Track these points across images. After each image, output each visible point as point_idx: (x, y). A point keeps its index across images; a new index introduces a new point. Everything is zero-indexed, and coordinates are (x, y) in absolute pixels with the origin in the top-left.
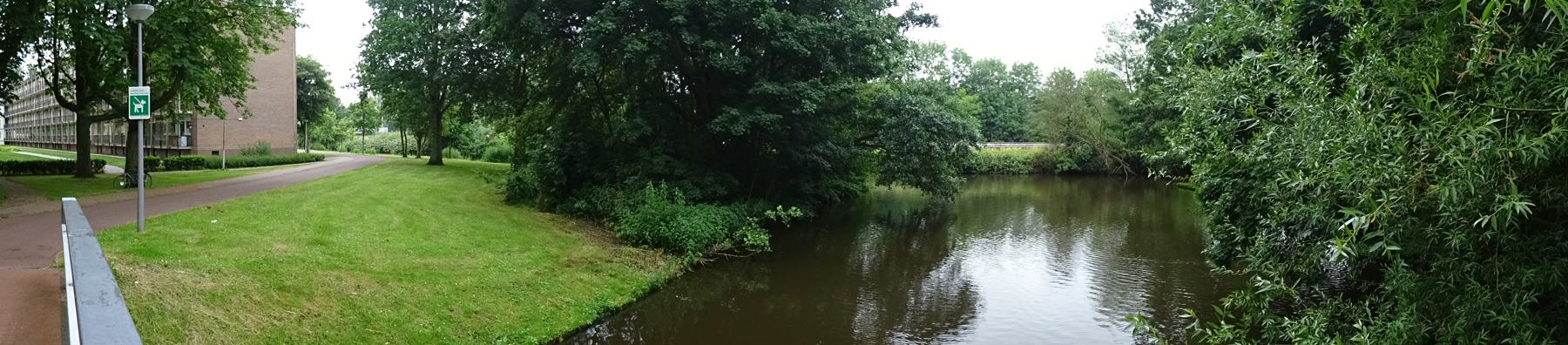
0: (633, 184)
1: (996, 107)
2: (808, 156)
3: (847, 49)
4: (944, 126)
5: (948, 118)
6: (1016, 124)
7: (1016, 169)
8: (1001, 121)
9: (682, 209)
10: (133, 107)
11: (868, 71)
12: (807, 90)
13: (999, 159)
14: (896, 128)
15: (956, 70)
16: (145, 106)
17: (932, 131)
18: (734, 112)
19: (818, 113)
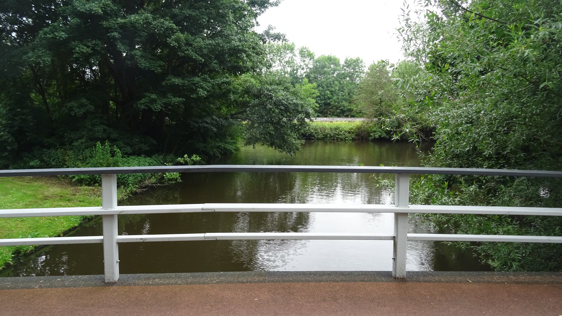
0: (79, 146)
1: (331, 92)
2: (201, 125)
3: (226, 56)
4: (289, 105)
5: (292, 100)
6: (345, 104)
7: (343, 137)
8: (335, 102)
9: (120, 159)
11: (237, 70)
12: (200, 82)
13: (331, 129)
14: (258, 106)
15: (302, 64)
17: (280, 109)
18: (153, 96)
19: (206, 98)
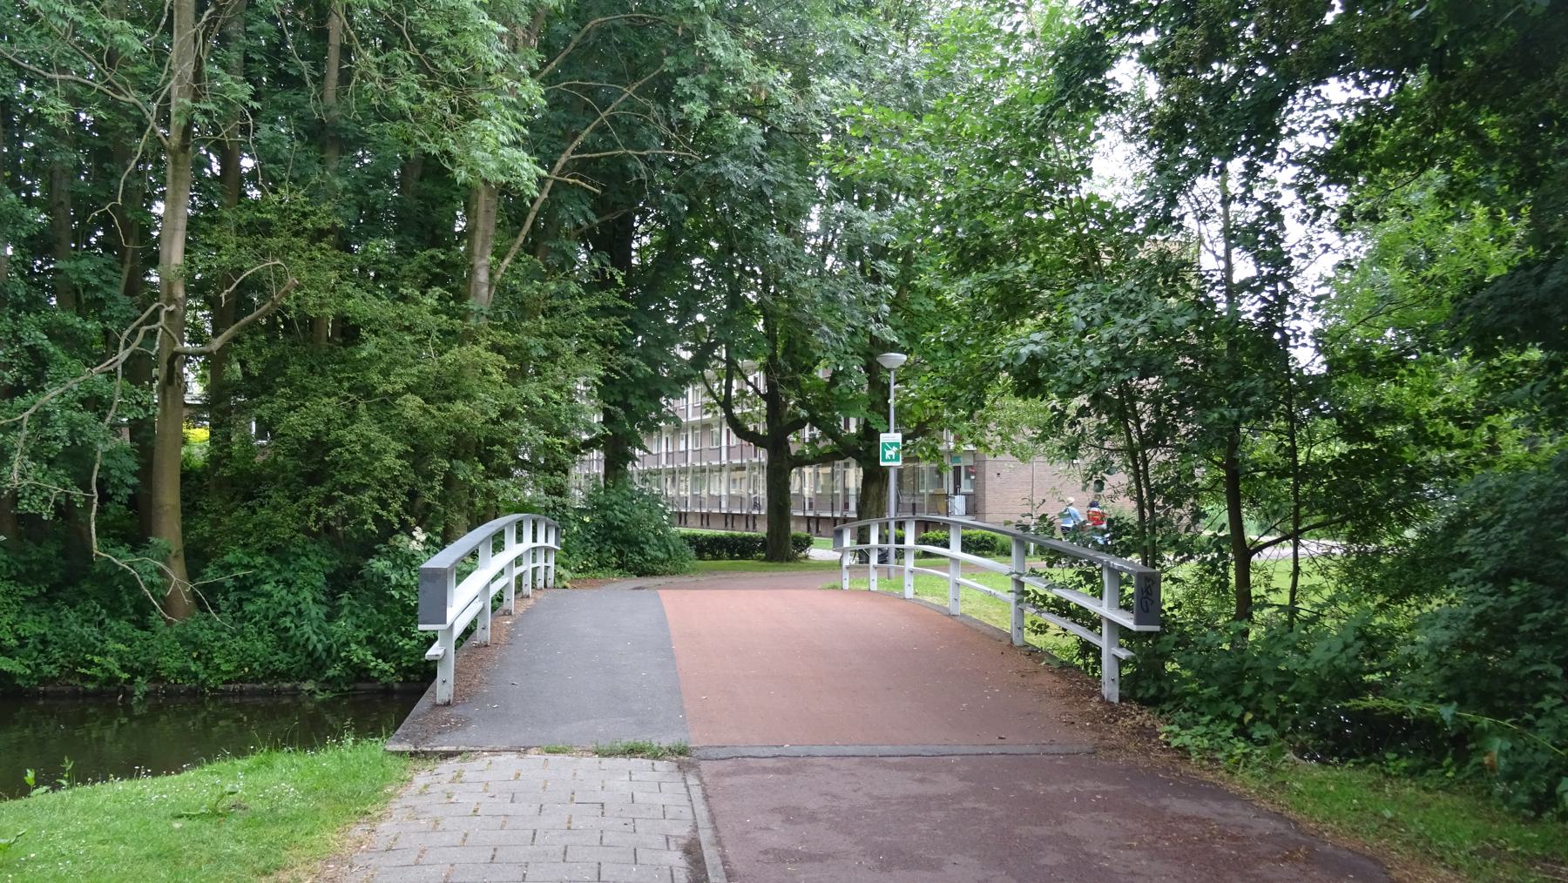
10: (884, 453)
16: (897, 453)
